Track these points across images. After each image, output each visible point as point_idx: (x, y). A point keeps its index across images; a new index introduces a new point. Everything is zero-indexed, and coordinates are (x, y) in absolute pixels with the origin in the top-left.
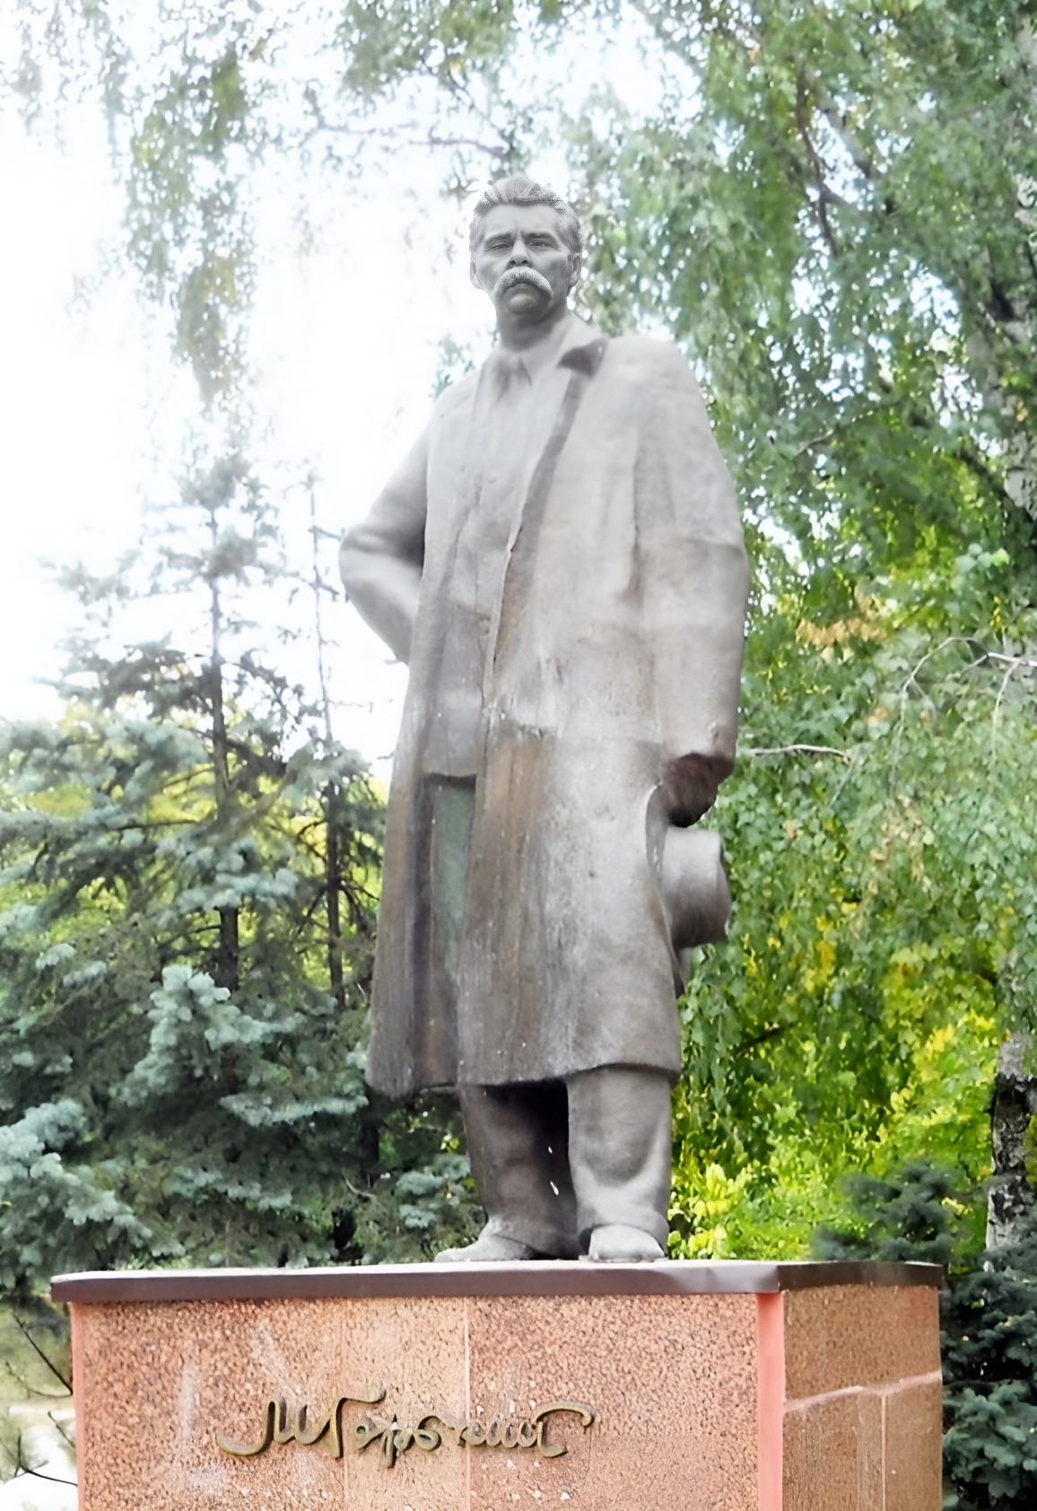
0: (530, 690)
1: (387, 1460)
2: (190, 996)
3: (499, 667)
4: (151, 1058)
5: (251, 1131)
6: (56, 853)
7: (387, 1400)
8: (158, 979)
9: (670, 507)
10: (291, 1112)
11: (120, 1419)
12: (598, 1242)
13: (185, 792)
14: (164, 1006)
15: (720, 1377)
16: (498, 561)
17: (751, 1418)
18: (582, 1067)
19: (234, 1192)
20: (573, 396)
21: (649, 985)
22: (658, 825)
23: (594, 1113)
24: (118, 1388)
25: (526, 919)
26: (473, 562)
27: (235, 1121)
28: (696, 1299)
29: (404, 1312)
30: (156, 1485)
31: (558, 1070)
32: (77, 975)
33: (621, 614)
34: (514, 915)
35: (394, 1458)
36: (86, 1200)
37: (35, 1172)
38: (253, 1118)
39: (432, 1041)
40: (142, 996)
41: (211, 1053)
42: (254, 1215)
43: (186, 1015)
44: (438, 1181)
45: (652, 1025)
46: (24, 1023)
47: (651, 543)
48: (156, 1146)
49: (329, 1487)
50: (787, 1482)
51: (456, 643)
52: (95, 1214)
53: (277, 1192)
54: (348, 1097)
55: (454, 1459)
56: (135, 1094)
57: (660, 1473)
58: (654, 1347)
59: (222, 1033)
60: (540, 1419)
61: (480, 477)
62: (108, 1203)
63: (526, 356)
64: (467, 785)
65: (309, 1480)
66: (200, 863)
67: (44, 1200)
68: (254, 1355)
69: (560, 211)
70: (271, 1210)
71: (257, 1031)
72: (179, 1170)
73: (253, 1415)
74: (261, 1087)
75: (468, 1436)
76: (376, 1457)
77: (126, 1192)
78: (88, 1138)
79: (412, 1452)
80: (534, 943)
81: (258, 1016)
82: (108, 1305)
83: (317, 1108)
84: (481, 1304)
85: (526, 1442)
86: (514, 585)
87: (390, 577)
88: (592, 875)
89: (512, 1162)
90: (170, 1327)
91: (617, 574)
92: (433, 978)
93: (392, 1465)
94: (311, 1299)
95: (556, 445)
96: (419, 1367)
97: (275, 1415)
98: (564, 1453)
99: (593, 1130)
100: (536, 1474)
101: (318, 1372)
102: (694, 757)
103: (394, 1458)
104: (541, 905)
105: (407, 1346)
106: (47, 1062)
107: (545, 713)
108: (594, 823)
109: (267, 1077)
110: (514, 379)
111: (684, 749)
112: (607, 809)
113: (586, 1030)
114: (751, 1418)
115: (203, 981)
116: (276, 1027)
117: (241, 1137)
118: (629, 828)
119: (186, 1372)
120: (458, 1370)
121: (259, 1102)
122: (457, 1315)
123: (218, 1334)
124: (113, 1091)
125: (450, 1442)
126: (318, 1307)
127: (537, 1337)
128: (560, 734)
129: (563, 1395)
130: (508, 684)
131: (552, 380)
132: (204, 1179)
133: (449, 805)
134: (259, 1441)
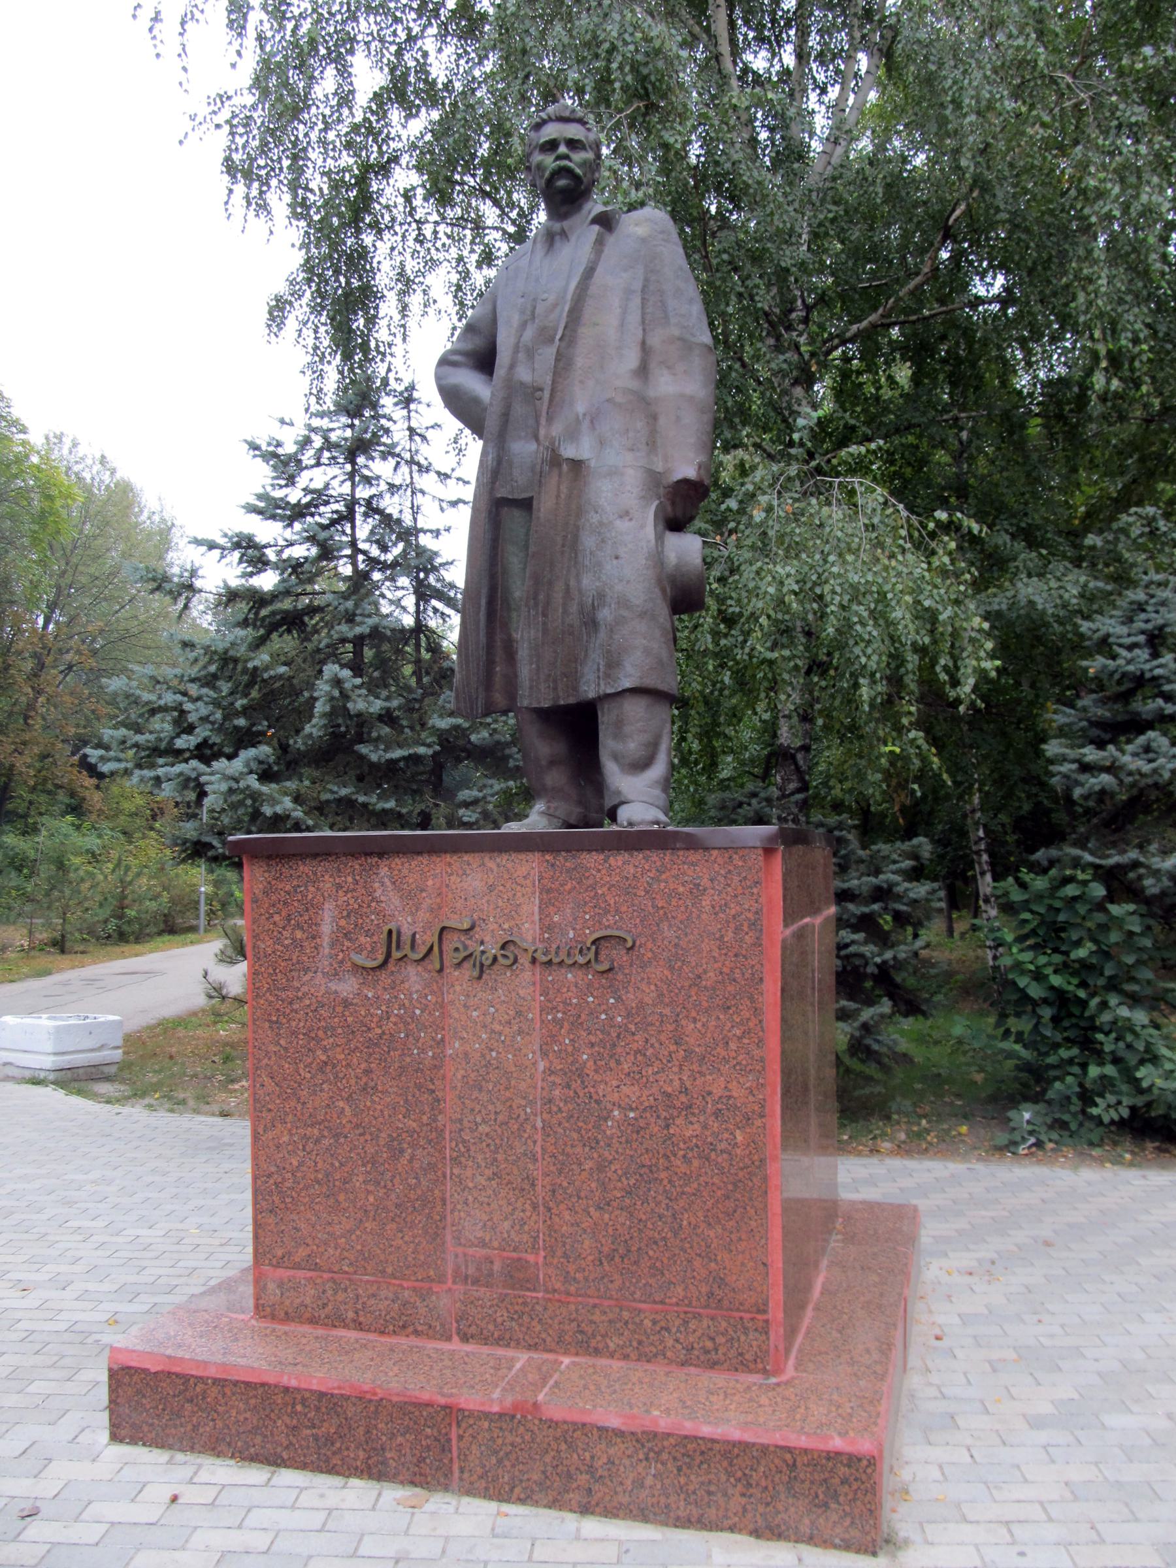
0: (573, 434)
1: (476, 973)
2: (337, 682)
3: (550, 419)
4: (314, 721)
5: (372, 765)
6: (259, 609)
7: (477, 929)
8: (320, 672)
9: (666, 317)
10: (397, 753)
11: (278, 941)
12: (624, 814)
13: (333, 430)
14: (323, 687)
15: (733, 912)
16: (549, 353)
17: (757, 943)
18: (609, 691)
19: (362, 799)
20: (600, 243)
21: (657, 633)
22: (661, 527)
23: (619, 724)
24: (277, 918)
25: (567, 590)
26: (531, 353)
27: (362, 758)
28: (715, 853)
29: (491, 864)
30: (305, 989)
31: (591, 695)
32: (272, 673)
33: (634, 384)
34: (559, 587)
35: (482, 972)
36: (274, 802)
37: (242, 784)
38: (374, 757)
39: (498, 680)
40: (311, 686)
41: (351, 717)
42: (373, 813)
43: (336, 693)
44: (481, 795)
45: (661, 662)
46: (240, 703)
47: (655, 341)
48: (316, 774)
49: (433, 993)
50: (783, 990)
51: (519, 409)
52: (279, 809)
53: (387, 800)
54: (429, 746)
55: (527, 975)
56: (305, 744)
57: (687, 984)
58: (681, 889)
59: (359, 704)
60: (593, 943)
61: (535, 300)
62: (288, 803)
63: (566, 224)
64: (526, 505)
65: (417, 987)
66: (346, 611)
67: (249, 802)
68: (377, 895)
69: (589, 130)
70: (384, 810)
71: (377, 706)
72: (329, 786)
73: (375, 938)
74: (379, 739)
75: (538, 955)
76: (468, 971)
77: (297, 799)
78: (276, 768)
79: (495, 967)
80: (574, 608)
81: (377, 697)
82: (269, 857)
83: (411, 751)
84: (547, 857)
85: (581, 960)
86: (561, 364)
87: (472, 382)
88: (617, 558)
89: (552, 763)
90: (315, 874)
91: (632, 359)
92: (499, 638)
93: (480, 977)
94: (420, 853)
95: (589, 273)
96: (500, 903)
97: (392, 938)
98: (610, 970)
99: (618, 735)
100: (590, 984)
101: (424, 906)
102: (685, 481)
103: (482, 972)
104: (579, 581)
105: (491, 888)
106: (253, 725)
107: (581, 449)
108: (618, 523)
109: (382, 733)
110: (557, 238)
111: (678, 476)
112: (627, 513)
113: (613, 664)
114: (757, 943)
115: (346, 673)
116: (387, 704)
117: (366, 769)
118: (643, 527)
119: (326, 906)
120: (531, 907)
121: (377, 748)
122: (529, 866)
123: (350, 879)
124: (291, 742)
125: (524, 960)
126: (424, 859)
127: (590, 882)
128: (593, 464)
129: (610, 925)
130: (557, 429)
131: (585, 235)
132: (344, 792)
133: (514, 519)
134: (381, 958)
